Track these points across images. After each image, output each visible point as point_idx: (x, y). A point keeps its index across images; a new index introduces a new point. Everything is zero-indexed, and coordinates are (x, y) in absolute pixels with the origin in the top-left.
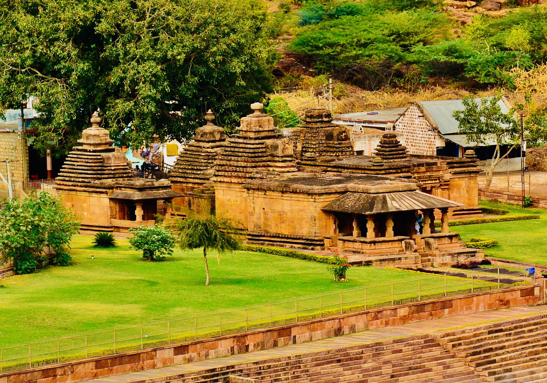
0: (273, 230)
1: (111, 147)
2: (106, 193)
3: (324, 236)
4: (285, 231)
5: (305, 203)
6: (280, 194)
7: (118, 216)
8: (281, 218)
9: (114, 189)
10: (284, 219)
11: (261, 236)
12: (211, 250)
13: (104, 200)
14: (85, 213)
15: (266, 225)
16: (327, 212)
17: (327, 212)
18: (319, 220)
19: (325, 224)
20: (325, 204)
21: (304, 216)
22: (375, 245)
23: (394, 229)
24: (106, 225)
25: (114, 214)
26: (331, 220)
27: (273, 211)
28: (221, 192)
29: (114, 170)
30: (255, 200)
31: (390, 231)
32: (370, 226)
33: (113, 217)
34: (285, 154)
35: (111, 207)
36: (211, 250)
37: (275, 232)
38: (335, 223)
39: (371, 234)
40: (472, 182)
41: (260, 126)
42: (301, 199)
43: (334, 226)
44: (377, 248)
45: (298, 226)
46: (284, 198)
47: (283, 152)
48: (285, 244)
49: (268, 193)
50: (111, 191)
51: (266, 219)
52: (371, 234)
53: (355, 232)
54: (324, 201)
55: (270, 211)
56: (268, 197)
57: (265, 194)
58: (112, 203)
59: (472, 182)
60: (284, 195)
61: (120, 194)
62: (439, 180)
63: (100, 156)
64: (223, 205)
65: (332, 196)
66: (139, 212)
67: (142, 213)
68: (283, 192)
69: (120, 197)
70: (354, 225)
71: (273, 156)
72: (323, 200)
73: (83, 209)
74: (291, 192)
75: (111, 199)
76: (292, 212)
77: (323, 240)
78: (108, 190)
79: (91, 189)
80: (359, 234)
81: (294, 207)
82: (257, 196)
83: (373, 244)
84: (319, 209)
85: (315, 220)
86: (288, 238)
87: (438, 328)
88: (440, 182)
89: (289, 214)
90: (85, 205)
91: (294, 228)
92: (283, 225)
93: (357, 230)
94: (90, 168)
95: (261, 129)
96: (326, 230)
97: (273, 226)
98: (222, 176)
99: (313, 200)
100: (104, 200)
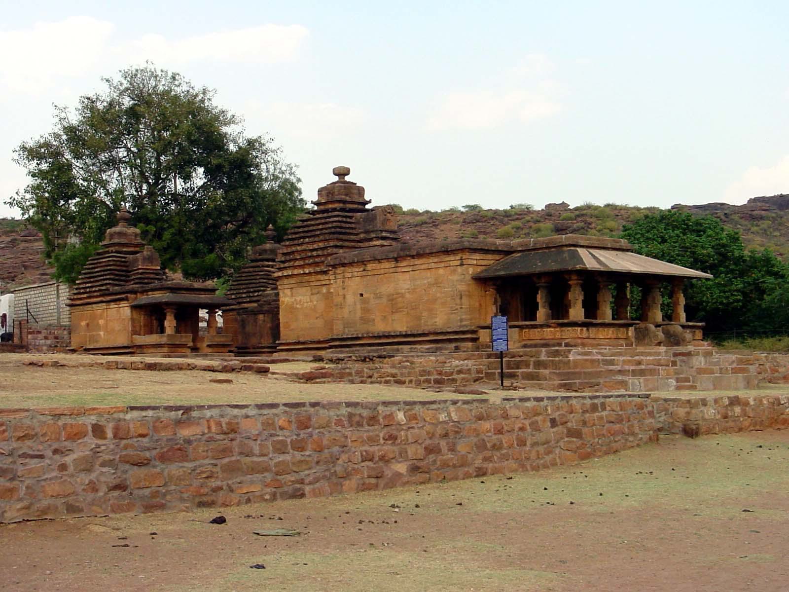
0: (380, 327)
2: (126, 299)
3: (477, 324)
4: (400, 325)
6: (393, 264)
7: (142, 332)
8: (394, 304)
10: (400, 305)
11: (357, 338)
12: (232, 121)
13: (124, 310)
14: (102, 333)
15: (365, 320)
16: (482, 281)
17: (482, 281)
18: (470, 296)
19: (477, 304)
20: (479, 269)
21: (438, 295)
24: (125, 345)
25: (138, 329)
26: (488, 298)
27: (378, 296)
28: (288, 292)
29: (141, 274)
30: (346, 284)
33: (135, 332)
34: (387, 228)
35: (133, 320)
36: (232, 121)
37: (383, 330)
38: (495, 303)
39: (577, 312)
41: (346, 195)
42: (433, 265)
43: (494, 308)
44: (592, 336)
45: (425, 314)
46: (399, 270)
47: (383, 224)
48: (400, 347)
49: (369, 267)
50: (133, 296)
51: (366, 310)
52: (577, 312)
53: (542, 313)
54: (476, 264)
55: (372, 295)
56: (370, 273)
57: (364, 270)
58: (134, 312)
60: (399, 265)
61: (143, 299)
63: (125, 258)
64: (292, 309)
65: (490, 256)
66: (170, 323)
67: (174, 323)
68: (396, 260)
69: (143, 302)
70: (539, 300)
71: (367, 232)
72: (475, 262)
73: (98, 327)
74: (413, 257)
75: (134, 308)
76: (413, 291)
78: (129, 295)
79: (109, 298)
80: (547, 315)
81: (418, 283)
82: (350, 275)
84: (468, 277)
85: (461, 298)
86: (406, 336)
89: (408, 296)
90: (101, 322)
91: (419, 318)
92: (397, 316)
93: (544, 307)
94: (108, 272)
95: (348, 199)
96: (480, 314)
97: (378, 319)
98: (289, 267)
99: (458, 263)
100: (124, 310)
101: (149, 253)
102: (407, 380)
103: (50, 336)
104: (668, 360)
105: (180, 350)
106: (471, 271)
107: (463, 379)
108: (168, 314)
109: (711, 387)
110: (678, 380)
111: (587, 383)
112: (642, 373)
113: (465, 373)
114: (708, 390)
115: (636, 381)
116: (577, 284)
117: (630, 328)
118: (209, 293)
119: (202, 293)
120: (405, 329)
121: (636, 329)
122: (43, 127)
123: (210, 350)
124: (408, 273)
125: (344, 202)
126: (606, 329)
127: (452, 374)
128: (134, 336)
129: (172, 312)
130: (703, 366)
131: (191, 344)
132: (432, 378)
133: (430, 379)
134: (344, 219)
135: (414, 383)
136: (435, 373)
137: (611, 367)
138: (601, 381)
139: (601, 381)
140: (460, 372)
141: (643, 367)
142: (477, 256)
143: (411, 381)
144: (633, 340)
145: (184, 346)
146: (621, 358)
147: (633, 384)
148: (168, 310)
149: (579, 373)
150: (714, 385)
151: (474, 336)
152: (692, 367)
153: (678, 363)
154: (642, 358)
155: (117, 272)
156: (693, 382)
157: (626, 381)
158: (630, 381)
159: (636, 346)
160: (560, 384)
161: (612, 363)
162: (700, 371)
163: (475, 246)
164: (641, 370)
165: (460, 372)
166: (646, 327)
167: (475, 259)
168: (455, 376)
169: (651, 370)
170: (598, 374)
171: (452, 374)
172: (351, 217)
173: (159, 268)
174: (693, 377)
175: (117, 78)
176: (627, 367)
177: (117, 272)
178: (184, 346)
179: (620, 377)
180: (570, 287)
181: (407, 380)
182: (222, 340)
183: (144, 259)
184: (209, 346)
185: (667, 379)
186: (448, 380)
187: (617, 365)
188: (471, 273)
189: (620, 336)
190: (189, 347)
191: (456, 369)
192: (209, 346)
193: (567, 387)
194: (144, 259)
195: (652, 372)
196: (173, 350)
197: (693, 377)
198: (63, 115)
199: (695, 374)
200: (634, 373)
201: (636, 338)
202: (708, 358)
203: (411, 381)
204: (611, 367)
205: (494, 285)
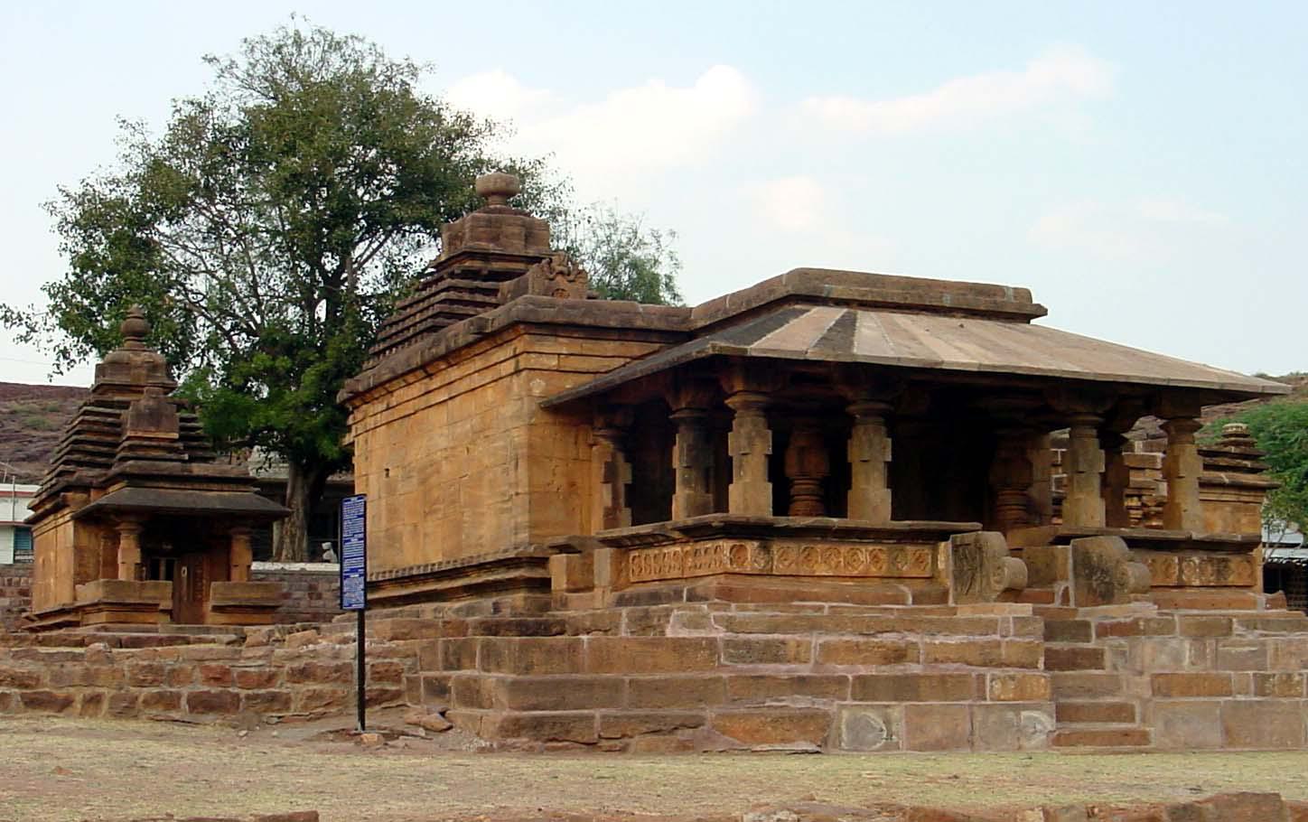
1: (194, 415)
3: (550, 541)
5: (490, 394)
9: (93, 493)
17: (573, 412)
19: (559, 481)
22: (765, 548)
23: (895, 477)
31: (873, 498)
32: (749, 447)
35: (78, 550)
38: (610, 476)
40: (1244, 520)
44: (779, 567)
59: (1244, 520)
62: (1140, 496)
65: (610, 347)
67: (136, 556)
70: (676, 464)
72: (553, 362)
77: (542, 562)
83: (752, 546)
84: (528, 406)
87: (983, 351)
88: (1144, 505)
93: (686, 483)
95: (492, 247)
101: (151, 403)
102: (79, 698)
103: (8, 590)
104: (1030, 649)
105: (140, 616)
106: (539, 386)
107: (314, 696)
108: (123, 535)
109: (1216, 737)
110: (1062, 714)
111: (645, 719)
112: (905, 688)
113: (326, 679)
114: (1197, 748)
115: (871, 714)
116: (747, 406)
117: (943, 544)
118: (234, 486)
119: (215, 487)
120: (440, 559)
121: (956, 548)
122: (107, 165)
123: (222, 618)
124: (443, 408)
125: (486, 257)
126: (844, 549)
127: (271, 679)
128: (77, 586)
129: (131, 531)
130: (1186, 666)
131: (166, 604)
132: (185, 691)
133: (179, 696)
134: (467, 296)
135: (105, 706)
136: (198, 674)
137: (768, 669)
138: (710, 713)
139: (710, 713)
140: (303, 674)
141: (916, 669)
142: (563, 345)
143: (95, 700)
144: (949, 583)
145: (151, 608)
146: (817, 639)
147: (857, 727)
148: (122, 526)
149: (616, 686)
150: (1227, 732)
151: (538, 573)
152: (1141, 673)
153: (1108, 659)
154: (912, 638)
155: (90, 447)
156: (1143, 720)
157: (826, 715)
158: (845, 714)
159: (1078, 604)
160: (517, 720)
161: (773, 653)
162: (1165, 685)
163: (547, 315)
164: (907, 677)
165: (303, 674)
166: (977, 541)
167: (553, 351)
168: (282, 687)
169: (943, 679)
170: (703, 692)
171: (271, 679)
172: (494, 292)
173: (176, 436)
174: (1145, 702)
175: (230, 49)
176: (840, 669)
177: (90, 447)
178: (151, 608)
179: (801, 703)
180: (731, 413)
181: (79, 695)
182: (253, 595)
183: (139, 416)
184: (216, 609)
185: (1017, 709)
186: (248, 697)
187: (796, 659)
188: (537, 392)
189: (905, 569)
190: (163, 611)
191: (288, 666)
192: (216, 609)
193: (547, 731)
194: (139, 416)
195: (946, 686)
196: (122, 616)
197: (1145, 702)
198: (138, 139)
199: (1148, 694)
200: (865, 688)
201: (956, 578)
202: (1210, 642)
203: (95, 700)
204: (768, 669)
205: (609, 425)
